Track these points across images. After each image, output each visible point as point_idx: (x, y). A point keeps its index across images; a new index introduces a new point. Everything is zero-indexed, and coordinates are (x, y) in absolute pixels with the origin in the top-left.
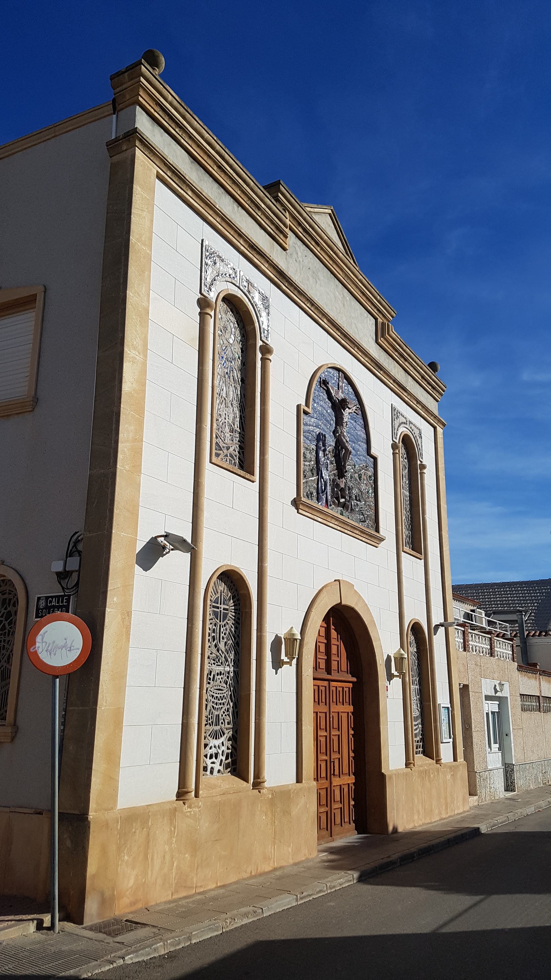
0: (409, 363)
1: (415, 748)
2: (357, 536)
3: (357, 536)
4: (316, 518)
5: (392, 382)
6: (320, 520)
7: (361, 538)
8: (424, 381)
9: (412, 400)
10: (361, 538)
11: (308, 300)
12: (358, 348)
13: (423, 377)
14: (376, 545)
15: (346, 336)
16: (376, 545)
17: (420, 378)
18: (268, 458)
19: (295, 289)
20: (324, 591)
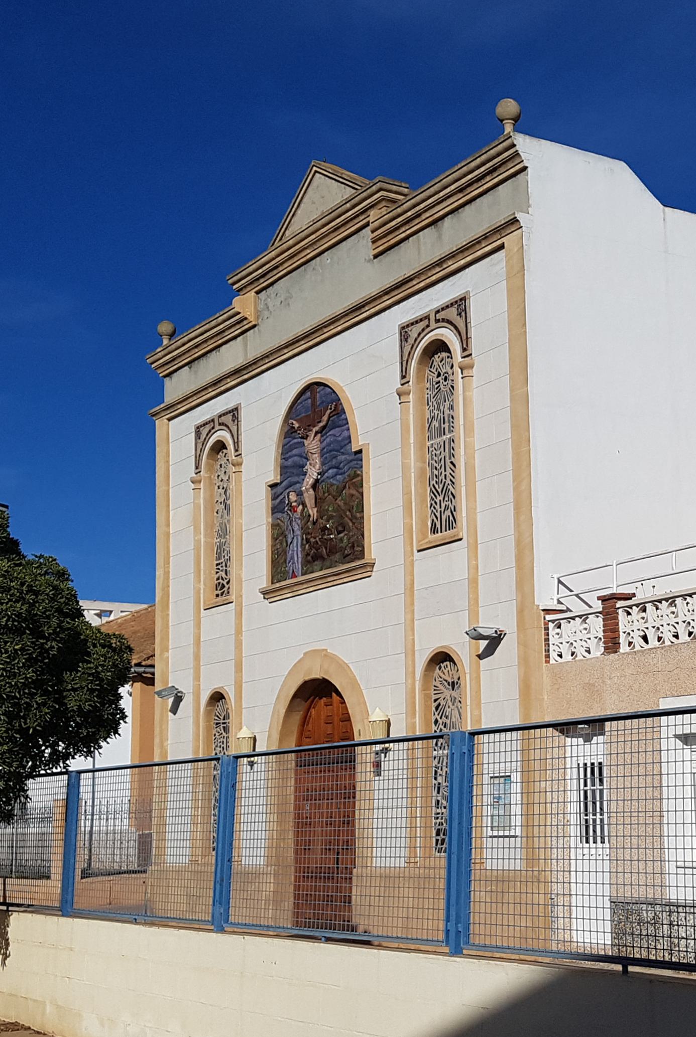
0: (426, 211)
1: (446, 840)
2: (335, 583)
3: (335, 583)
4: (284, 596)
5: (386, 297)
6: (289, 595)
7: (341, 581)
8: (469, 190)
9: (445, 266)
10: (341, 581)
11: (478, 243)
12: (325, 327)
13: (461, 190)
14: (369, 574)
15: (307, 336)
16: (369, 574)
17: (461, 195)
18: (267, 541)
19: (247, 367)
20: (22, 1032)
